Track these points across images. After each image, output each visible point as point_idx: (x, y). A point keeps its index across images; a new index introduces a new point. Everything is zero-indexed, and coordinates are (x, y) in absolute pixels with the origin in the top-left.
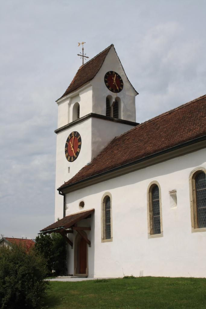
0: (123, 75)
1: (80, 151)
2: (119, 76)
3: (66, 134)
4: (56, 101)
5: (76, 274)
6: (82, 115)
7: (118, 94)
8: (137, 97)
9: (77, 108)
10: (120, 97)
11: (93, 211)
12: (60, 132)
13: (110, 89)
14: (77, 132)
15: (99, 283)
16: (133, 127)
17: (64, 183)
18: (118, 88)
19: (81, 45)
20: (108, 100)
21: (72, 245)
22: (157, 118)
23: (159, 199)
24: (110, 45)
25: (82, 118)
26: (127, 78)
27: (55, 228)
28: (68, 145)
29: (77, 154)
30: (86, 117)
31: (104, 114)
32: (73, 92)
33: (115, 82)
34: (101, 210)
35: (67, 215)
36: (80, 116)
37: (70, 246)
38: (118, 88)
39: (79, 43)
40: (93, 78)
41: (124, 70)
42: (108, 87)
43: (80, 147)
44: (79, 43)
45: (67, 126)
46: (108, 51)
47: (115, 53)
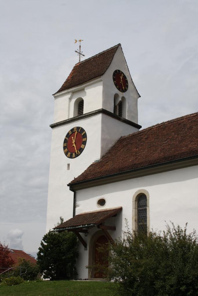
1: (84, 147)
3: (67, 128)
4: (53, 95)
5: (92, 279)
6: (86, 110)
7: (124, 93)
8: (139, 99)
9: (80, 104)
11: (120, 210)
12: (57, 127)
13: (117, 87)
14: (81, 128)
17: (73, 179)
18: (123, 88)
19: (78, 43)
20: (116, 96)
21: (85, 246)
23: (147, 208)
24: (117, 44)
25: (86, 114)
26: (132, 80)
27: (80, 225)
28: (67, 141)
29: (81, 150)
30: (95, 112)
31: (112, 111)
32: (77, 86)
33: (121, 81)
34: (133, 209)
35: (77, 214)
36: (84, 111)
37: (82, 247)
38: (123, 88)
39: (75, 40)
40: (104, 74)
41: (129, 71)
42: (116, 85)
43: (85, 143)
44: (75, 40)
45: (67, 121)
46: (117, 50)
47: (122, 52)
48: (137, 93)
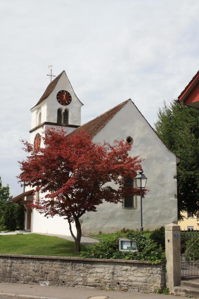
0: (72, 92)
2: (68, 93)
3: (34, 134)
7: (67, 106)
8: (82, 107)
10: (68, 108)
15: (196, 110)
16: (75, 129)
18: (67, 102)
19: (50, 67)
20: (59, 111)
22: (120, 105)
26: (75, 94)
31: (56, 122)
33: (64, 97)
38: (67, 102)
42: (59, 102)
48: (80, 103)
